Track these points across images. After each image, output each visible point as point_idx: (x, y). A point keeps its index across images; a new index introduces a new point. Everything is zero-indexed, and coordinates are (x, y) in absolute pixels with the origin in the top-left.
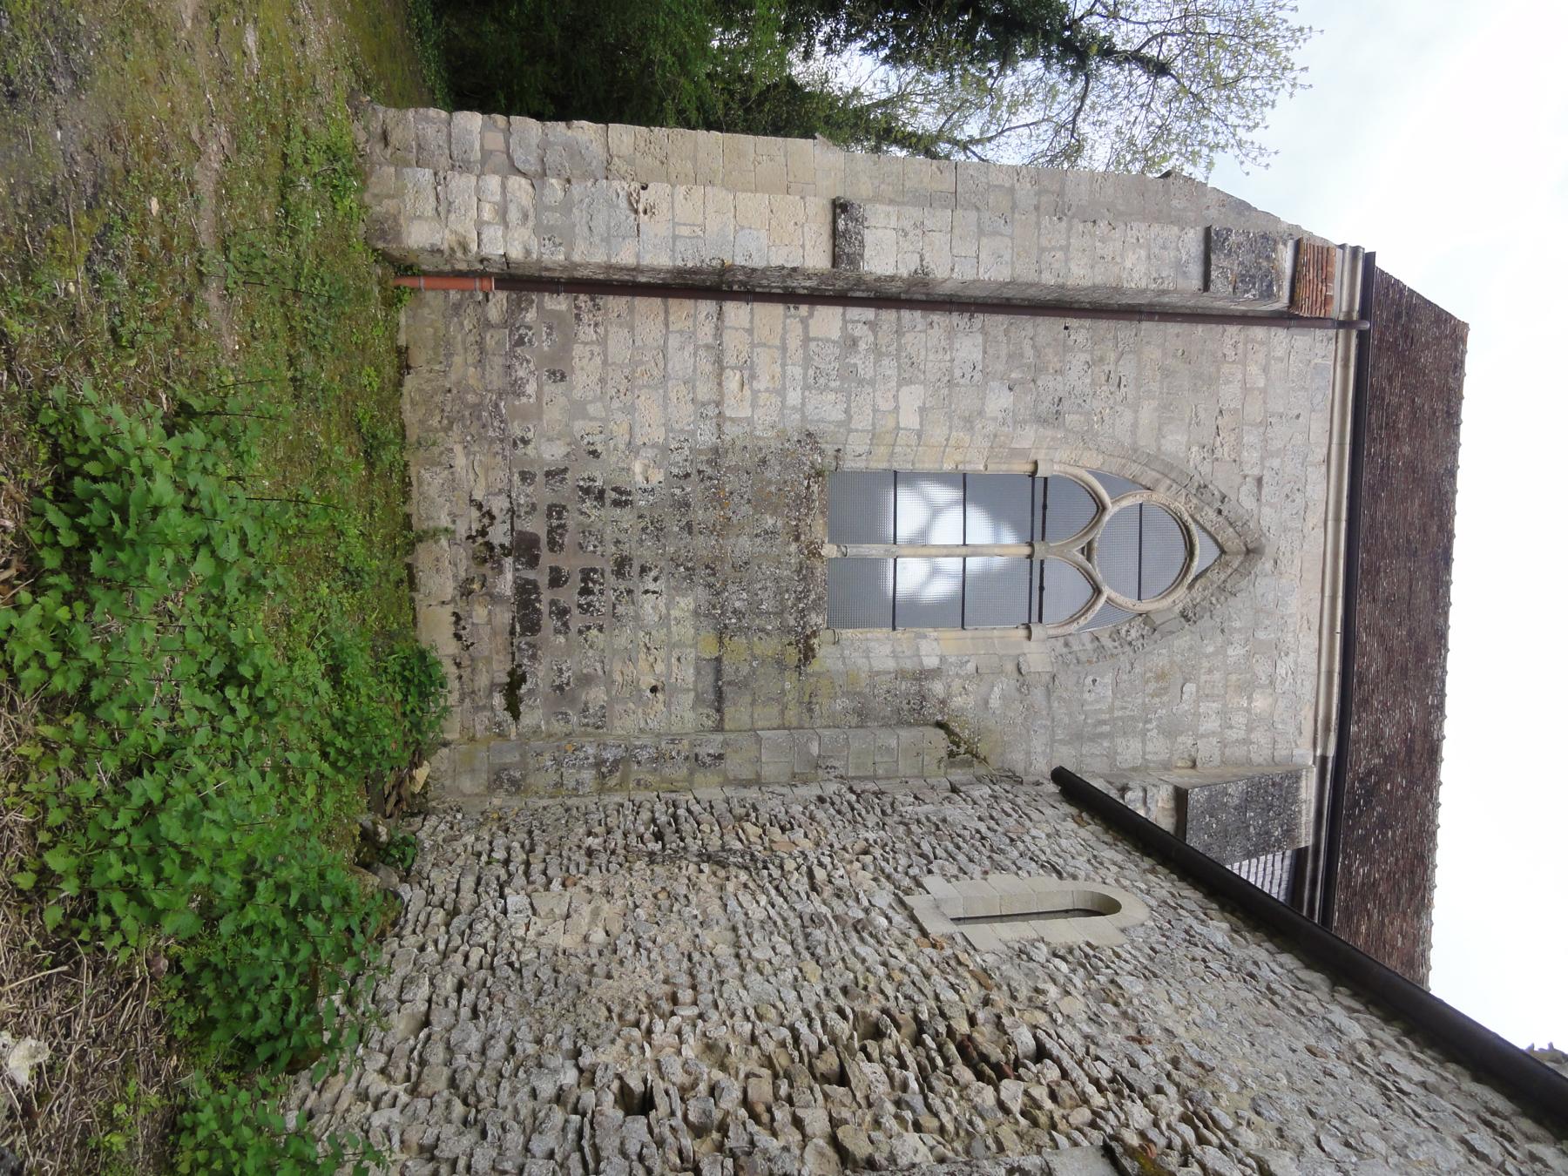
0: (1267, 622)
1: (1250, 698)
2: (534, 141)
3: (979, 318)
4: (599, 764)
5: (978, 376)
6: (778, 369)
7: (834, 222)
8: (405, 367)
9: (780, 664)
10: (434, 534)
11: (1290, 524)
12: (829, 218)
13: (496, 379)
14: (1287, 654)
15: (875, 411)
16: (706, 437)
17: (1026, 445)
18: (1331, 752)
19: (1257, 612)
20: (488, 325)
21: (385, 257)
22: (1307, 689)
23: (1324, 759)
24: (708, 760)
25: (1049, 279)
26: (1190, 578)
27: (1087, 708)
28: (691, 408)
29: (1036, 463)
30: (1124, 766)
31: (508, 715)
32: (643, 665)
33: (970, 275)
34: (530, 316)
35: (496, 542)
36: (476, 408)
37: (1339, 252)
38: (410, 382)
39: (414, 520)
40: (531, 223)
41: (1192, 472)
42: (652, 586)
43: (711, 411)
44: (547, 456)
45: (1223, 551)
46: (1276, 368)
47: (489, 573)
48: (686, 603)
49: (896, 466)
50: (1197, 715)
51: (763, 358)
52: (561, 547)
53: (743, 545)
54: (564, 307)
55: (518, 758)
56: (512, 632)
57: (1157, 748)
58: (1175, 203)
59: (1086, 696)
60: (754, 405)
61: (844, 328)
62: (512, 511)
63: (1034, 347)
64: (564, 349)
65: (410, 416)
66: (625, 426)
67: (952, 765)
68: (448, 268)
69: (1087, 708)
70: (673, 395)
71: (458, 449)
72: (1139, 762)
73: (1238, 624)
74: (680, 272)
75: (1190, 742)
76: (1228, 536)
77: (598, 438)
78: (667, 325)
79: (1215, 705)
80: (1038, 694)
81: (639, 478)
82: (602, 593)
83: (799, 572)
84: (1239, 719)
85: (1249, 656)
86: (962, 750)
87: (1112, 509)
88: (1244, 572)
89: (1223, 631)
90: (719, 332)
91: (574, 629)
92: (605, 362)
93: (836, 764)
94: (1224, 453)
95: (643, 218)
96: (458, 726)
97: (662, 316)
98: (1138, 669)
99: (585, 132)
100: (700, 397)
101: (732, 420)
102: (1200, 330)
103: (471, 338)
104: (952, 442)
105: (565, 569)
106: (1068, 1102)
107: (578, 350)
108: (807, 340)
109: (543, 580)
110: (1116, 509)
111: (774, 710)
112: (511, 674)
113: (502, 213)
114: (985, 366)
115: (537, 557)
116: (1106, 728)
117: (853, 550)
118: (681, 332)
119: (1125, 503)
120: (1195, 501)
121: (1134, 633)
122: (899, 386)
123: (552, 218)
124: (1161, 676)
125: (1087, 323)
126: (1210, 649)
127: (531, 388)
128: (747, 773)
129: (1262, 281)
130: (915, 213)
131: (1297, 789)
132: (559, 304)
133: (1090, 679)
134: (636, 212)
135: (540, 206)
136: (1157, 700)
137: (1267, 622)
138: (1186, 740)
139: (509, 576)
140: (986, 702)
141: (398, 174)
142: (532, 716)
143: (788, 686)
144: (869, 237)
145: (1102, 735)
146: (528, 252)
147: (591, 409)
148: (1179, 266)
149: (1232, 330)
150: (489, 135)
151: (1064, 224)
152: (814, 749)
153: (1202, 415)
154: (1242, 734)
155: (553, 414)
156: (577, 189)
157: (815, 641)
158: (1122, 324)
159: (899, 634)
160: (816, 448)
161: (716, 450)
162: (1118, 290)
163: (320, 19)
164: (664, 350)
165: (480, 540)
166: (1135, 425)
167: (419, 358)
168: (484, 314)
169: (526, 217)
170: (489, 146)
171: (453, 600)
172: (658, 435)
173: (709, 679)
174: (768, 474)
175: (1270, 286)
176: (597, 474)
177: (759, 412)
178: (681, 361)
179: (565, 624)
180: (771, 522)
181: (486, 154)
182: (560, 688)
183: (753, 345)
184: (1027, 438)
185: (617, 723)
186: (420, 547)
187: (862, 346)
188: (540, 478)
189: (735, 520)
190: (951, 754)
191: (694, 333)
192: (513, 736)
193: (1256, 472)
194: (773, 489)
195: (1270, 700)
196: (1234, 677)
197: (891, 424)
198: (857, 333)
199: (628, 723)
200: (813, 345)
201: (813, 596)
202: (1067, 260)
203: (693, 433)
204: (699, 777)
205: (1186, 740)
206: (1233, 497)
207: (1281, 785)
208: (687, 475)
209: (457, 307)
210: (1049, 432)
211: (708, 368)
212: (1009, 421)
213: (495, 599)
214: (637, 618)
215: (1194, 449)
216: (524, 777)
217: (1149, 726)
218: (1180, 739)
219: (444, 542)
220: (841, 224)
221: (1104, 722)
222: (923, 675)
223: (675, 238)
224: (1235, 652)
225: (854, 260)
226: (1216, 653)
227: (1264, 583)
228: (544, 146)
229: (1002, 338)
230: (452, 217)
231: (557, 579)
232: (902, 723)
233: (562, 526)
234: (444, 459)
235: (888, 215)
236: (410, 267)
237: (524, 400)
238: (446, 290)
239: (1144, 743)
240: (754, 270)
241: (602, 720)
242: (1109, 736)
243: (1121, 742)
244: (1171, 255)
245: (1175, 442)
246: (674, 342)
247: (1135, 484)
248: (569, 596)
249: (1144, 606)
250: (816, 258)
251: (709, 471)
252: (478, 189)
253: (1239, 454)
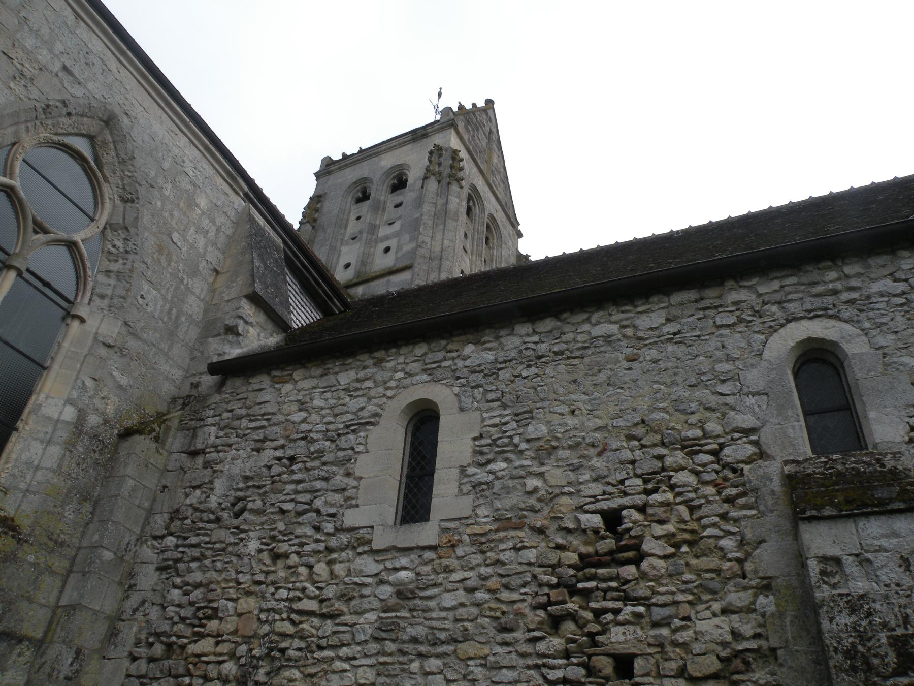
0: (160, 155)
1: (197, 206)
14: (184, 162)
18: (246, 188)
23: (246, 194)
24: (76, 666)
27: (156, 315)
30: (201, 316)
57: (199, 286)
75: (204, 263)
79: (192, 230)
80: (132, 343)
86: (158, 429)
87: (16, 183)
89: (152, 186)
93: (126, 540)
98: (149, 260)
106: (668, 515)
110: (18, 179)
111: (47, 579)
116: (174, 311)
119: (17, 170)
120: (49, 122)
121: (119, 244)
124: (160, 249)
126: (159, 204)
128: (102, 628)
133: (139, 298)
136: (173, 263)
137: (160, 155)
140: (120, 387)
143: (31, 558)
145: (177, 318)
154: (214, 228)
190: (157, 439)
195: (203, 195)
196: (182, 205)
206: (68, 97)
215: (12, 85)
217: (185, 282)
218: (201, 268)
221: (170, 310)
224: (168, 191)
249: (103, 219)
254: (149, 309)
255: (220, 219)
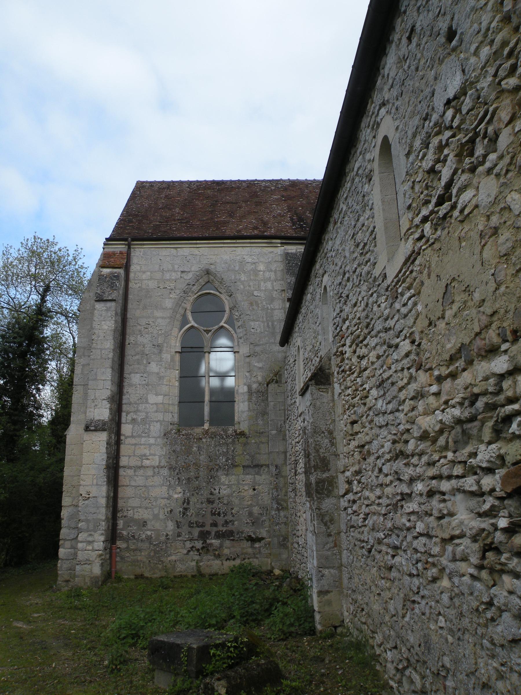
1: (260, 271)
2: (68, 531)
3: (125, 375)
4: (278, 509)
5: (145, 375)
6: (142, 447)
7: (92, 430)
8: (142, 576)
9: (245, 444)
10: (198, 567)
11: (198, 260)
12: (90, 432)
13: (146, 545)
15: (156, 412)
16: (165, 472)
17: (169, 356)
18: (279, 241)
19: (229, 270)
20: (128, 548)
21: (104, 582)
22: (257, 250)
23: (281, 243)
24: (278, 471)
25: (111, 355)
26: (218, 293)
27: (262, 331)
28: (156, 477)
29: (176, 352)
31: (262, 542)
32: (245, 494)
33: (109, 383)
34: (125, 533)
35: (201, 546)
36: (156, 552)
37: (106, 250)
38: (147, 574)
39: (194, 574)
40: (93, 533)
41: (179, 296)
42: (217, 491)
43: (156, 470)
44: (172, 528)
45: (209, 282)
46: (144, 268)
47: (212, 548)
48: (223, 479)
49: (177, 403)
50: (265, 290)
51: (138, 452)
52: (203, 523)
53: (203, 458)
54: (122, 521)
55: (276, 538)
56: (233, 540)
58: (88, 308)
59: (258, 331)
60: (155, 455)
61: (128, 423)
62: (191, 540)
63: (135, 355)
64: (136, 522)
65: (157, 575)
66: (162, 500)
67: (281, 382)
68: (108, 561)
69: (262, 331)
70: (151, 484)
71: (169, 558)
72: (282, 311)
73: (233, 277)
74: (109, 482)
75: (275, 292)
76: (202, 282)
77: (166, 510)
78: (128, 486)
80: (257, 349)
81: (180, 495)
82: (219, 509)
83: (213, 438)
84: (267, 274)
85: (245, 272)
87: (193, 323)
88: (215, 276)
90: (130, 468)
91: (232, 518)
92: (140, 507)
94: (172, 285)
95: (91, 495)
96: (266, 559)
97: (125, 487)
98: (249, 313)
99: (65, 513)
100: (152, 474)
101: (160, 463)
102: (130, 297)
103: (132, 553)
104: (168, 383)
105: (211, 521)
107: (136, 517)
108: (132, 436)
109: (215, 529)
112: (248, 540)
113: (90, 543)
114: (142, 373)
115: (207, 531)
116: (270, 324)
117: (206, 417)
118: (130, 481)
119: (191, 318)
121: (237, 314)
122: (148, 403)
123: (91, 527)
124: (251, 304)
125: (127, 336)
126: (242, 287)
127: (149, 533)
128: (282, 456)
129: (113, 280)
130: (89, 402)
131: (292, 253)
132: (121, 523)
133: (252, 330)
134: (89, 498)
135: (87, 530)
136: (260, 305)
138: (275, 294)
139: (213, 541)
140: (260, 368)
141: (78, 577)
142: (263, 533)
143: (253, 441)
144: (97, 418)
145: (273, 325)
146: (102, 534)
147: (156, 512)
148: (107, 310)
149: (131, 285)
150: (66, 546)
151: (93, 350)
152: (274, 432)
153: (160, 294)
154: (273, 273)
155: (158, 525)
156: (82, 518)
157: (238, 431)
158: (128, 324)
159: (236, 400)
160: (170, 432)
161: (170, 469)
162: (115, 331)
163: (30, 600)
164: (136, 487)
165: (201, 551)
166: (162, 318)
167: (138, 571)
168: (124, 549)
169: (91, 535)
170: (69, 546)
171: (221, 561)
172: (165, 489)
173: (251, 470)
174: (178, 449)
175: (115, 276)
176: (178, 510)
177: (157, 453)
178: (140, 481)
179: (231, 521)
180: (195, 448)
181: (72, 547)
182: (253, 523)
183: (134, 456)
184: (166, 356)
185: (266, 503)
186: (203, 572)
187: (135, 417)
188: (179, 530)
189: (194, 461)
190: (277, 382)
191: (130, 476)
192: (269, 540)
193: (179, 273)
194: (183, 448)
196: (252, 277)
197: (161, 406)
198: (130, 419)
199: (266, 499)
200: (134, 434)
201: (222, 432)
202: (105, 349)
203: (164, 477)
204: (284, 474)
205: (275, 294)
207: (290, 260)
208: (179, 478)
209: (122, 558)
210: (165, 349)
211: (142, 471)
212: (160, 363)
213: (221, 546)
214: (228, 496)
215: (171, 296)
216: (282, 536)
219: (201, 564)
220: (92, 428)
221: (268, 324)
222: (250, 392)
223: (97, 485)
224: (243, 277)
225: (104, 423)
226: (243, 285)
227: (219, 268)
228: (69, 527)
229: (132, 367)
230: (91, 559)
231: (215, 524)
232: (267, 399)
233: (196, 522)
234: (173, 563)
235: (90, 411)
236: (108, 574)
237: (153, 535)
238: (116, 562)
239: (275, 309)
240: (108, 457)
241: (265, 509)
242: (273, 322)
243: (275, 318)
244: (104, 313)
245: (168, 303)
246: (133, 483)
247: (184, 316)
248: (220, 520)
250: (103, 436)
251: (177, 471)
252: (82, 550)
253: (173, 280)
254: (258, 331)
255: (274, 267)
